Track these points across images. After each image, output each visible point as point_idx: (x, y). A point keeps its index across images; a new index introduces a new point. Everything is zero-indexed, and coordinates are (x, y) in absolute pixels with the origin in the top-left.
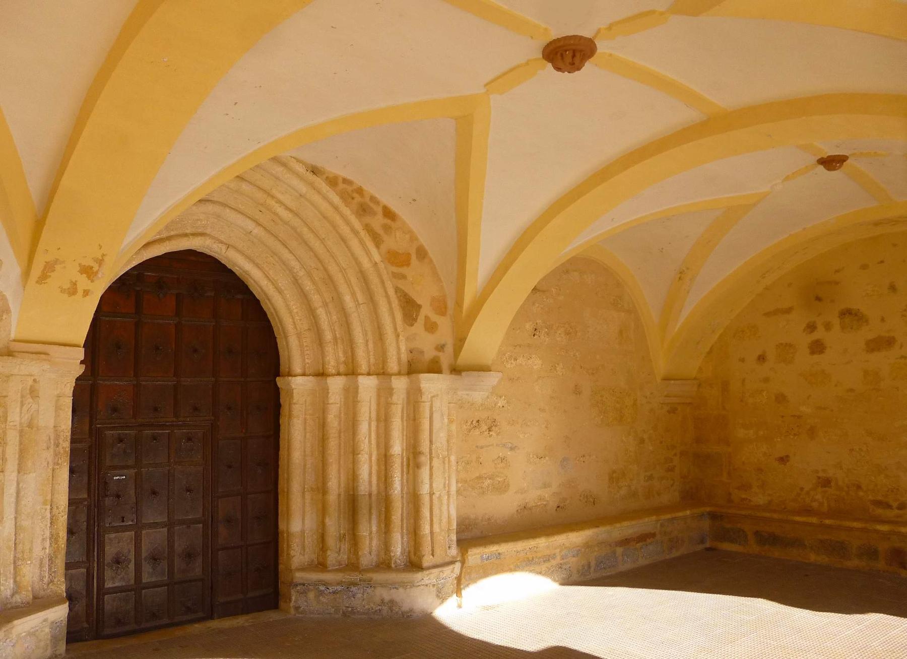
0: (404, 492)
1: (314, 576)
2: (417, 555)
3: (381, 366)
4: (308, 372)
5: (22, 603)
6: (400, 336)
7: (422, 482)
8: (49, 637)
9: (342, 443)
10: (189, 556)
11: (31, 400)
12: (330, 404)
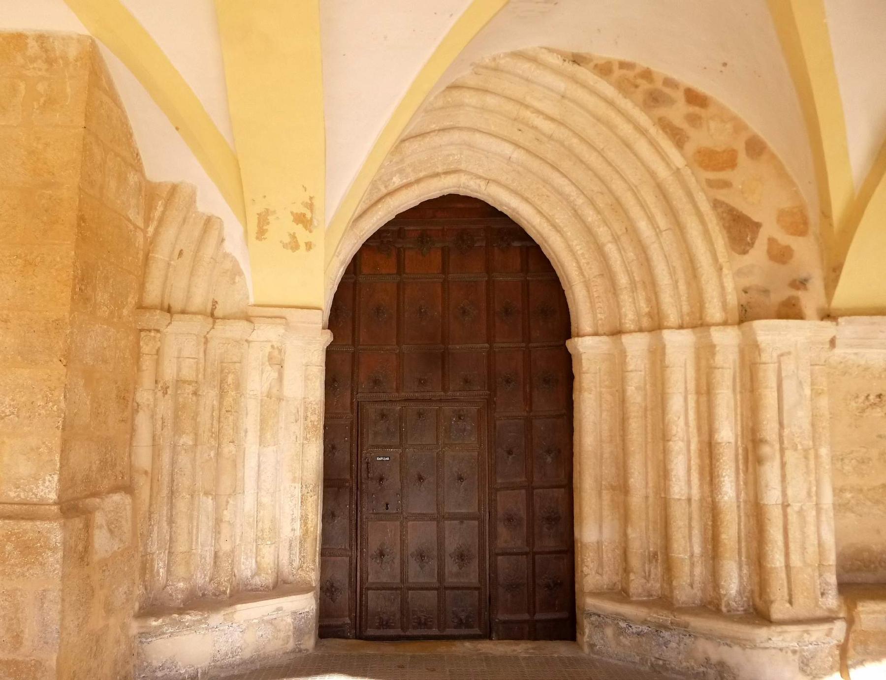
0: (741, 500)
1: (609, 607)
2: (763, 599)
3: (698, 315)
4: (600, 331)
5: (262, 587)
6: (724, 269)
7: (767, 486)
8: (291, 628)
9: (649, 425)
10: (462, 557)
11: (270, 368)
12: (627, 371)
